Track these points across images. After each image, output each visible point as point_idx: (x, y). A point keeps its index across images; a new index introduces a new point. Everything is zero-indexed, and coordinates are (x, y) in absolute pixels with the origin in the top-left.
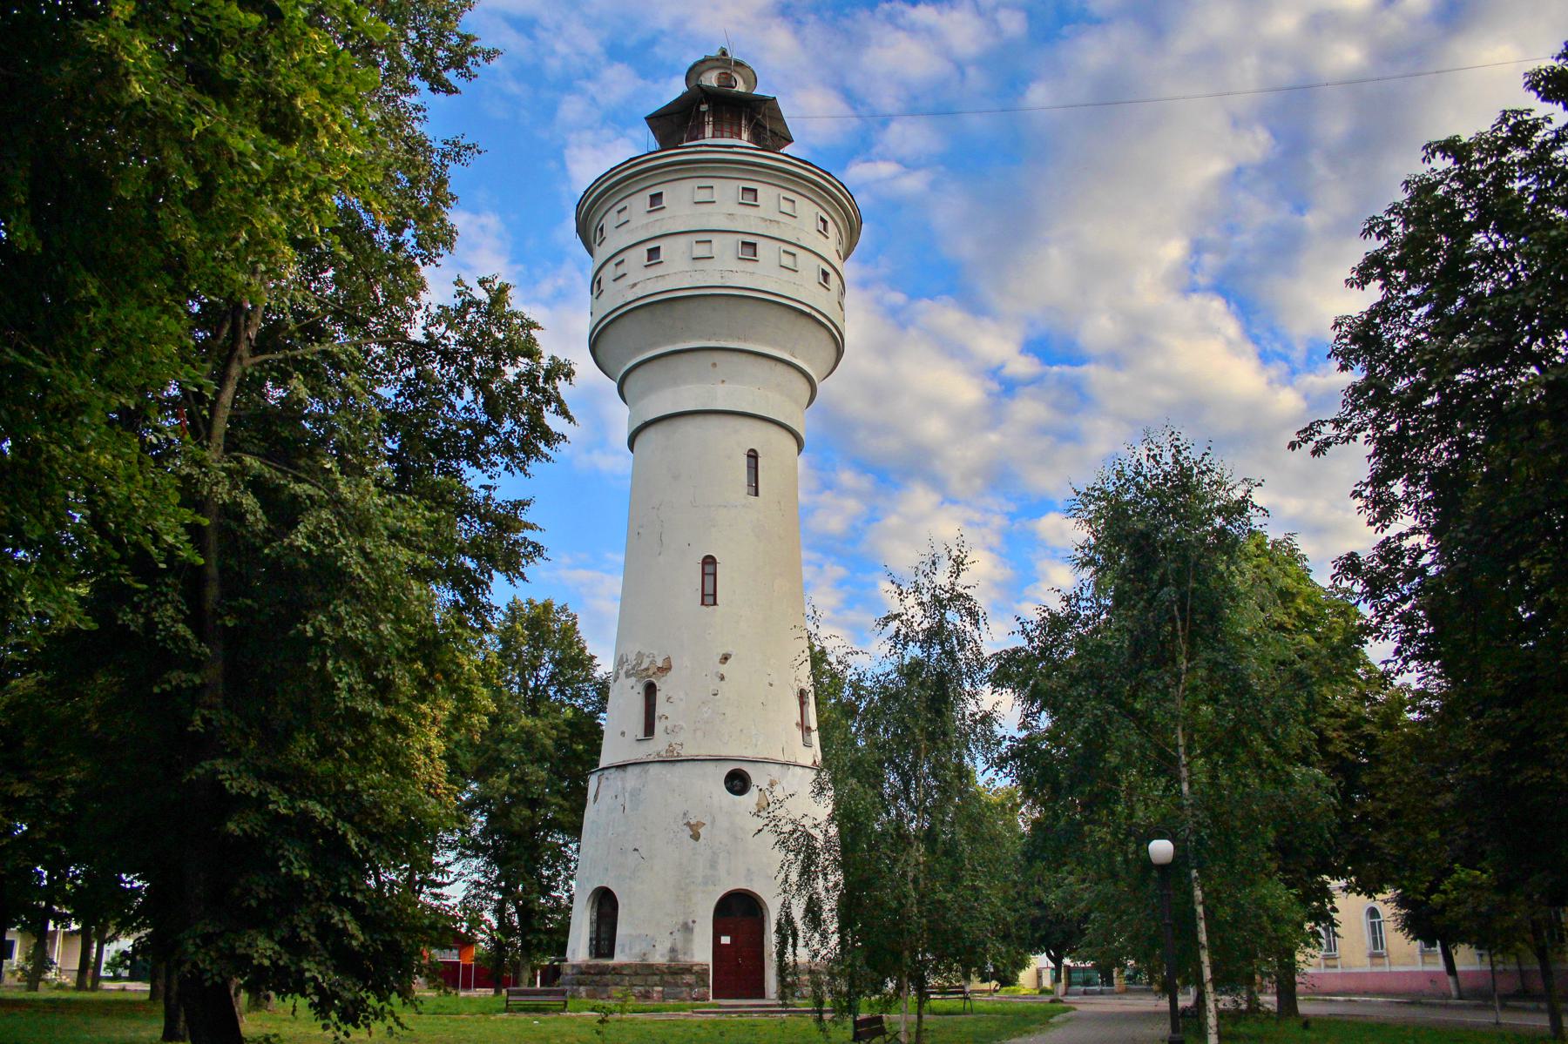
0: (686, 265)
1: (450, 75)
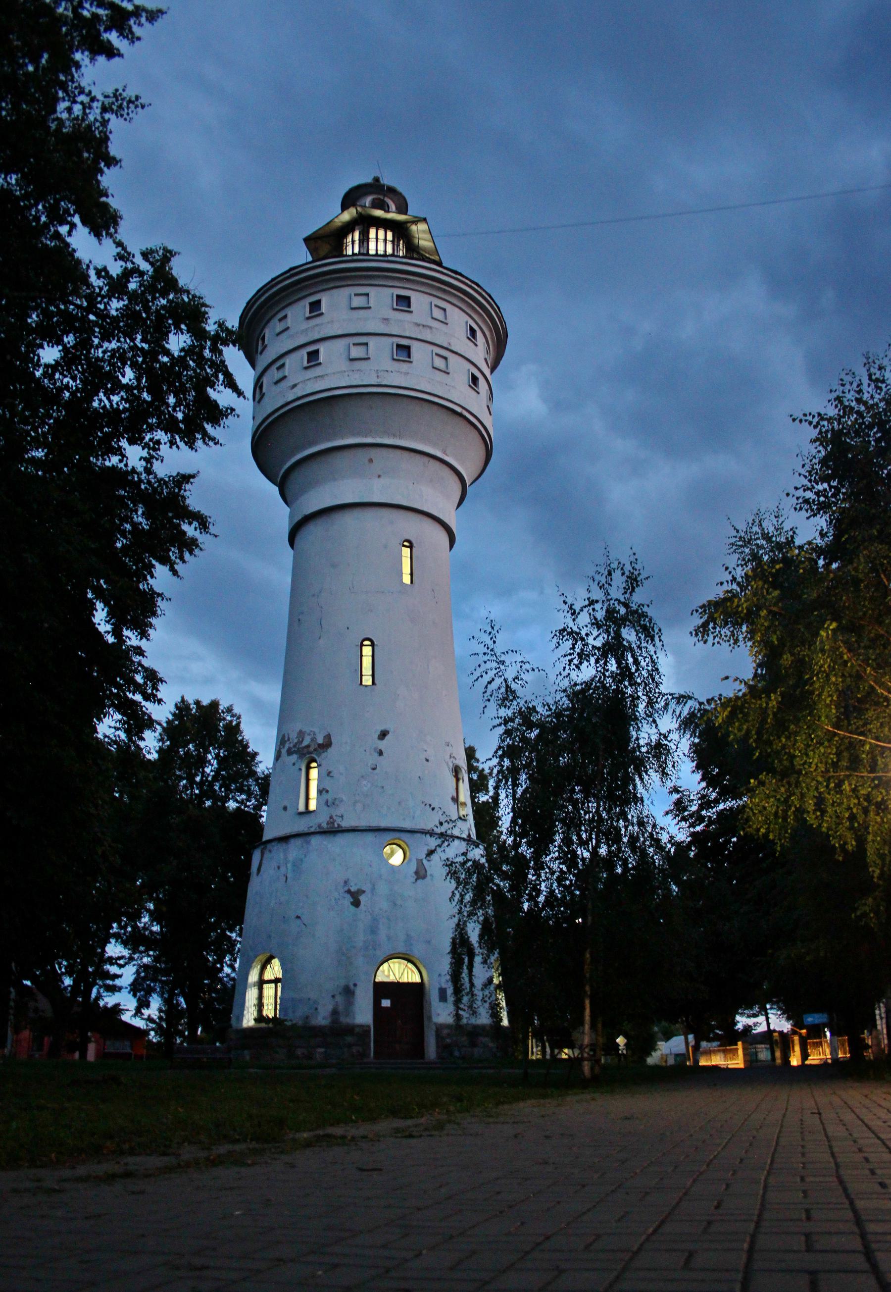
0: (344, 365)
1: (113, 37)
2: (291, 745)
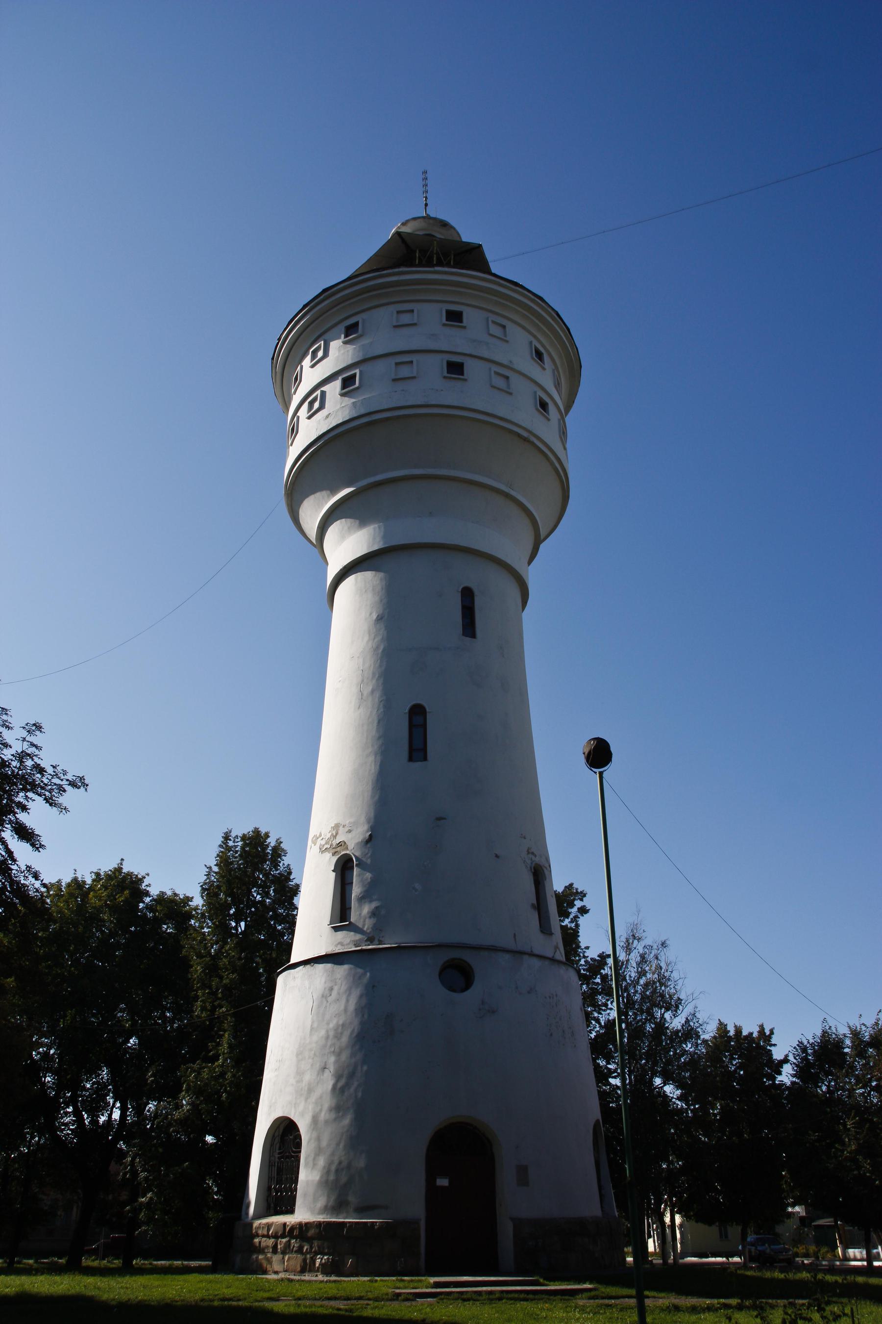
2: (323, 842)
